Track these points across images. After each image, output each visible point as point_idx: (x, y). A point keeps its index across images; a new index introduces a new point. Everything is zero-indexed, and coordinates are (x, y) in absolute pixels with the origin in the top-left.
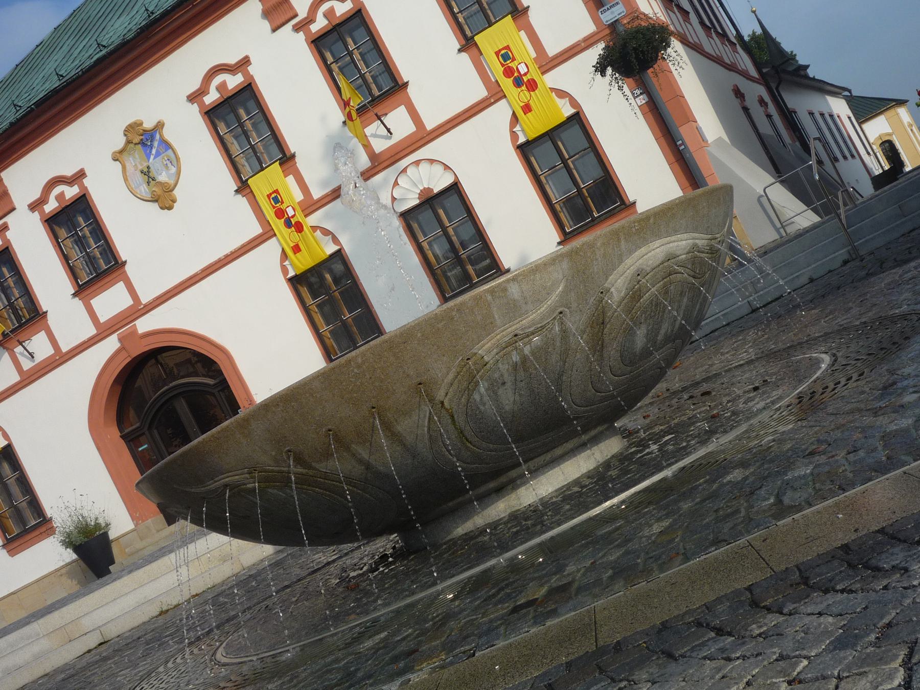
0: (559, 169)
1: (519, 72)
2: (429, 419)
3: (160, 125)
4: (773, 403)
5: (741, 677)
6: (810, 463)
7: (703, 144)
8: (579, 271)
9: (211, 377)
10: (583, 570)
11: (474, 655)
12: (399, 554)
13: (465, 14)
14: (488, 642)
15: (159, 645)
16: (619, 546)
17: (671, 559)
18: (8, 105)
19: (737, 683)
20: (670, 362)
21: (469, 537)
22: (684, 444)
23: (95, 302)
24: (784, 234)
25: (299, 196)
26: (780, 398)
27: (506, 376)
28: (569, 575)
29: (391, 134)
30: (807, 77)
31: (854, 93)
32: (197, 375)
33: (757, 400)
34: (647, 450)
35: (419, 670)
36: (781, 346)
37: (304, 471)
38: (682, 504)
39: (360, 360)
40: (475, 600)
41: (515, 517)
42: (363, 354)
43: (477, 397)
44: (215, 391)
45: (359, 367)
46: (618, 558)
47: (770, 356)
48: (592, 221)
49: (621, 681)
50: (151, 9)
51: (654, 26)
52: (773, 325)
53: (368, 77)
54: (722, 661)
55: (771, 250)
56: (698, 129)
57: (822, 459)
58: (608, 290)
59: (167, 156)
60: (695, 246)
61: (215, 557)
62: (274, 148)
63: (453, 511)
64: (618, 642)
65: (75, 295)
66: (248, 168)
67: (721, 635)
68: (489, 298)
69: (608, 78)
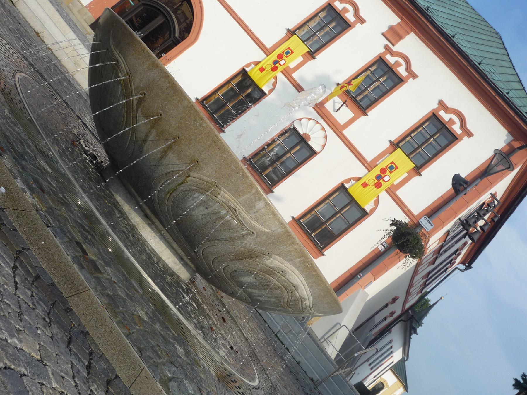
0: (334, 210)
1: (384, 177)
2: (178, 170)
4: (226, 360)
5: (64, 388)
7: (363, 287)
8: (278, 241)
11: (48, 227)
12: (98, 166)
13: (411, 140)
14: (57, 233)
15: (18, 37)
16: (127, 295)
17: (126, 327)
19: (61, 386)
20: (239, 298)
21: (116, 205)
22: (193, 316)
24: (321, 341)
25: (292, 65)
26: (229, 364)
27: (212, 209)
28: (105, 270)
30: (411, 334)
31: (406, 362)
33: (226, 350)
34: (185, 295)
35: (33, 197)
36: (258, 355)
37: (135, 105)
38: (158, 324)
39: (204, 125)
40: (80, 219)
41: (133, 229)
42: (208, 126)
43: (196, 195)
45: (200, 125)
47: (253, 354)
48: (309, 234)
49: (49, 318)
51: (423, 248)
52: (269, 348)
53: (366, 93)
54: (72, 374)
55: (311, 337)
58: (271, 257)
61: (75, 58)
62: (316, 46)
63: (130, 193)
64: (71, 310)
66: (303, 33)
67: (87, 369)
68: (254, 191)
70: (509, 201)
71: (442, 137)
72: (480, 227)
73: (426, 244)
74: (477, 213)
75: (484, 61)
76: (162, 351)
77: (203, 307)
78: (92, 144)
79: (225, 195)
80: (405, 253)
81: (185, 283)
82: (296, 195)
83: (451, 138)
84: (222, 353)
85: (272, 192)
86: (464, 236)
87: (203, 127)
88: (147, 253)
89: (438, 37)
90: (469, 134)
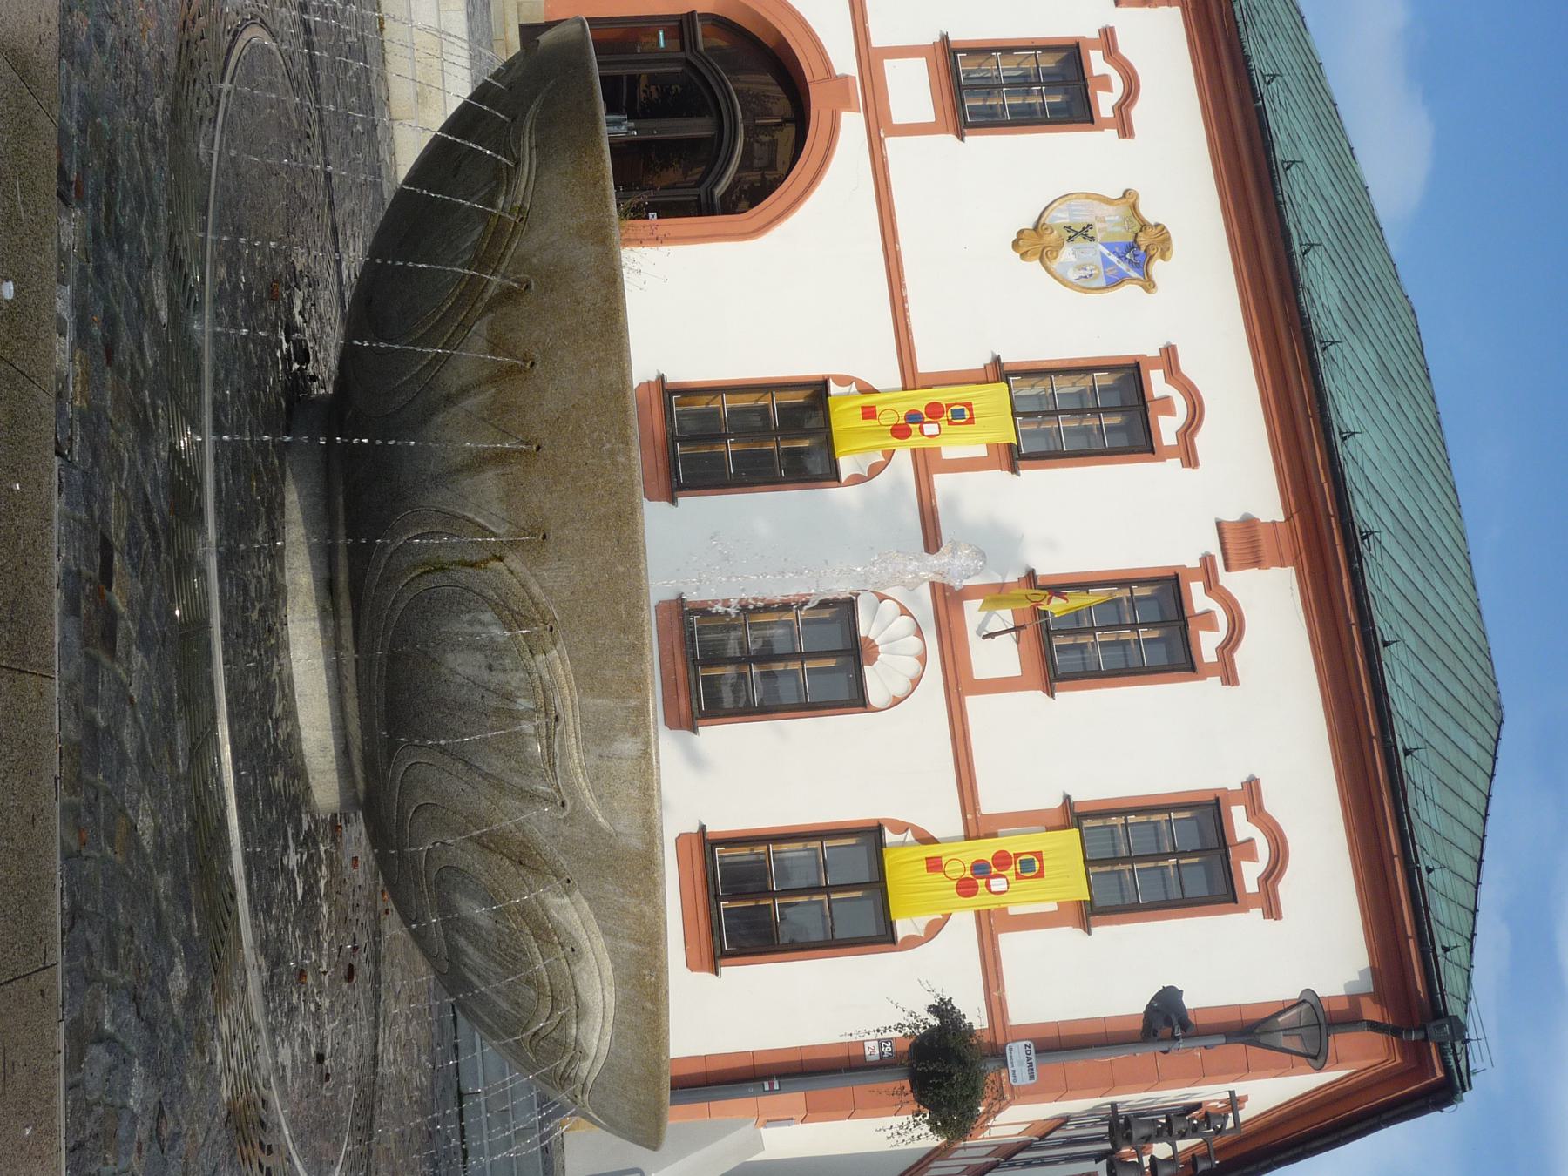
2: (484, 528)
3: (1149, 285)
4: (283, 1079)
6: (145, 1110)
7: (762, 1119)
9: (730, 190)
10: (125, 679)
11: (58, 453)
12: (297, 385)
16: (142, 751)
17: (79, 830)
18: (1280, 64)
20: (419, 937)
21: (274, 509)
23: (920, 64)
25: (949, 453)
26: (284, 1094)
28: (128, 654)
29: (985, 637)
32: (741, 168)
34: (292, 846)
37: (487, 296)
38: (169, 876)
39: (621, 459)
41: (276, 594)
42: (628, 468)
43: (487, 617)
44: (701, 191)
45: (612, 453)
46: (121, 744)
48: (717, 895)
50: (1332, 348)
53: (1088, 639)
56: (790, 1120)
57: (142, 1132)
58: (568, 892)
59: (1097, 276)
60: (584, 1057)
62: (1040, 446)
65: (945, 39)
68: (633, 703)
69: (924, 1015)
70: (1262, 1141)
71: (1201, 870)
72: (1153, 1159)
73: (990, 1113)
74: (1168, 1119)
75: (1421, 754)
76: (130, 951)
77: (318, 907)
78: (320, 318)
79: (556, 664)
80: (920, 1102)
81: (313, 817)
82: (743, 778)
83: (1221, 888)
84: (285, 1055)
85: (694, 730)
86: (1098, 1157)
87: (615, 464)
88: (268, 680)
89: (1348, 620)
90: (1272, 910)
